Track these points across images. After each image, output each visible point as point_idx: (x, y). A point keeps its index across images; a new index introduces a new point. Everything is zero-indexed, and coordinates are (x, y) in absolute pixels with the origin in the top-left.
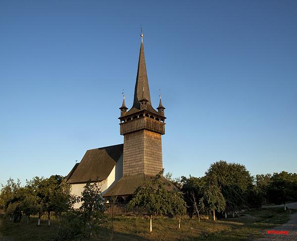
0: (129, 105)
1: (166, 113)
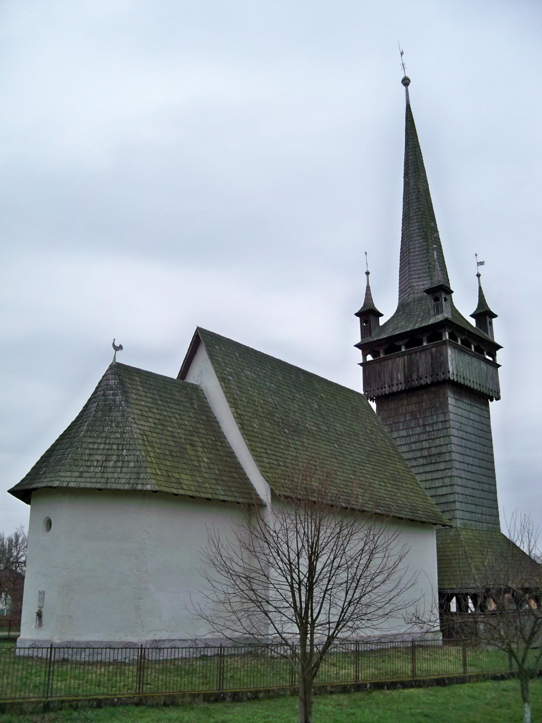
0: (387, 307)
1: (499, 332)
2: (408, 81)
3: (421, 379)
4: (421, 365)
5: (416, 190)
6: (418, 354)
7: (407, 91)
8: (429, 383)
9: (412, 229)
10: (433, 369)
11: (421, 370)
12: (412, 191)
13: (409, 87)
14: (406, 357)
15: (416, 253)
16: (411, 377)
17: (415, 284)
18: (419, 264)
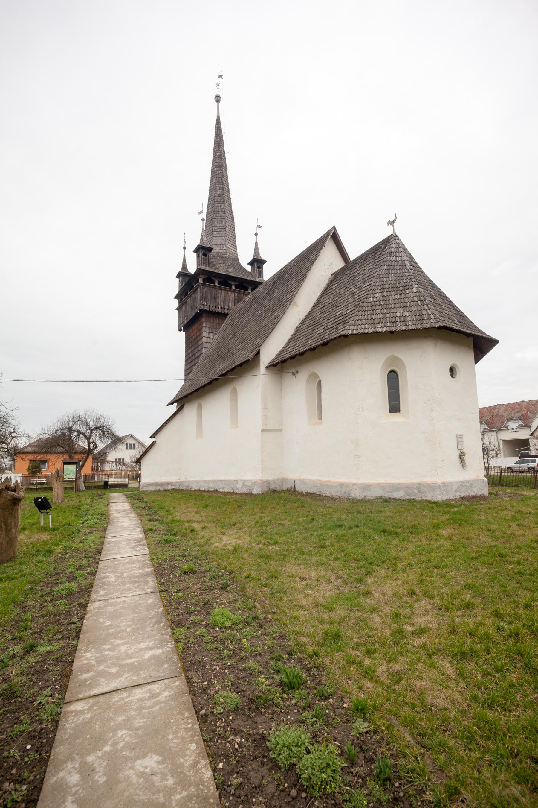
7: (218, 106)
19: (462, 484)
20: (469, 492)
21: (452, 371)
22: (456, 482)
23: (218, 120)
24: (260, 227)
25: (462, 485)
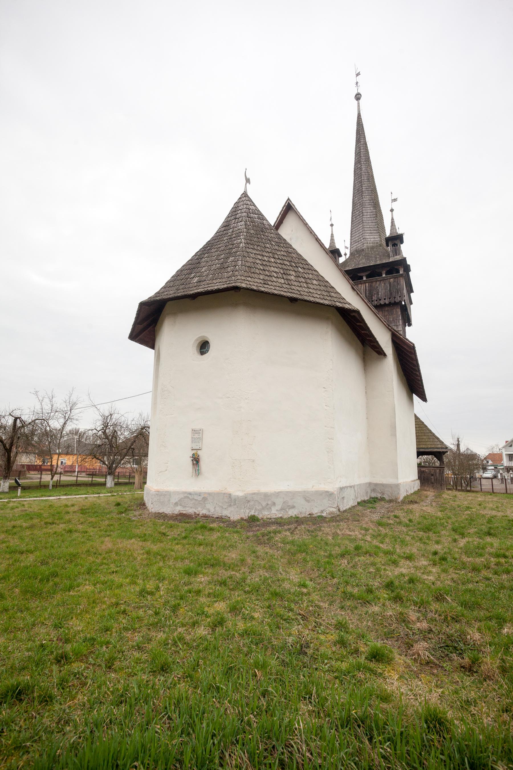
2: (360, 96)
3: (380, 300)
4: (380, 290)
5: (367, 174)
6: (378, 283)
7: (359, 104)
8: (387, 303)
9: (365, 199)
10: (391, 294)
11: (380, 293)
12: (364, 174)
13: (360, 101)
14: (367, 284)
15: (368, 216)
16: (372, 298)
17: (368, 237)
18: (370, 224)
19: (188, 496)
20: (199, 509)
21: (204, 347)
22: (178, 493)
23: (359, 116)
24: (395, 200)
25: (185, 497)
